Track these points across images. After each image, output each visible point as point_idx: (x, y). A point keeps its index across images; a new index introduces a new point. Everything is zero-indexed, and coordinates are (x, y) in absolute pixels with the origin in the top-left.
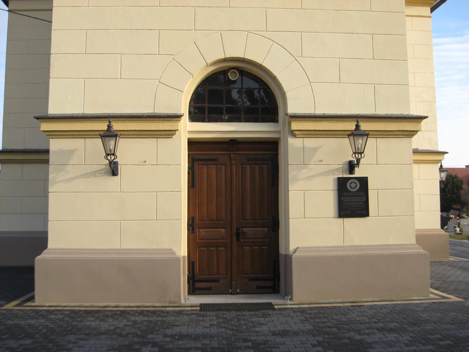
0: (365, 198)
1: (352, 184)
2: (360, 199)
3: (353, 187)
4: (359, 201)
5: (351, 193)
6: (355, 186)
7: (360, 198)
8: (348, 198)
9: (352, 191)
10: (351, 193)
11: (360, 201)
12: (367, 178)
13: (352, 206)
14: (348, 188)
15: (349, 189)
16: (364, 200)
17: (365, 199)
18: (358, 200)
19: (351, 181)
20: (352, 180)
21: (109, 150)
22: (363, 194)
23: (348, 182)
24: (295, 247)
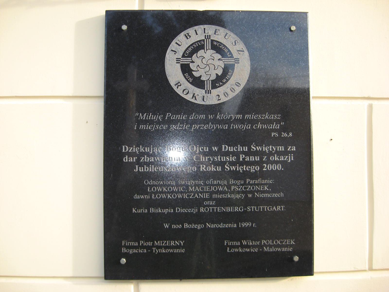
0: (286, 153)
1: (201, 53)
2: (257, 159)
3: (210, 52)
4: (246, 175)
5: (192, 118)
6: (220, 72)
7: (249, 153)
8: (244, 243)
9: (199, 101)
10: (192, 118)
11: (253, 169)
12: (306, 13)
13: (199, 203)
14: (172, 83)
15: (179, 91)
16: (279, 167)
17: (290, 159)
18: (244, 163)
19: (194, 38)
20: (200, 28)
21: (174, 158)
22: (274, 126)
23: (173, 45)
24: (175, 151)
